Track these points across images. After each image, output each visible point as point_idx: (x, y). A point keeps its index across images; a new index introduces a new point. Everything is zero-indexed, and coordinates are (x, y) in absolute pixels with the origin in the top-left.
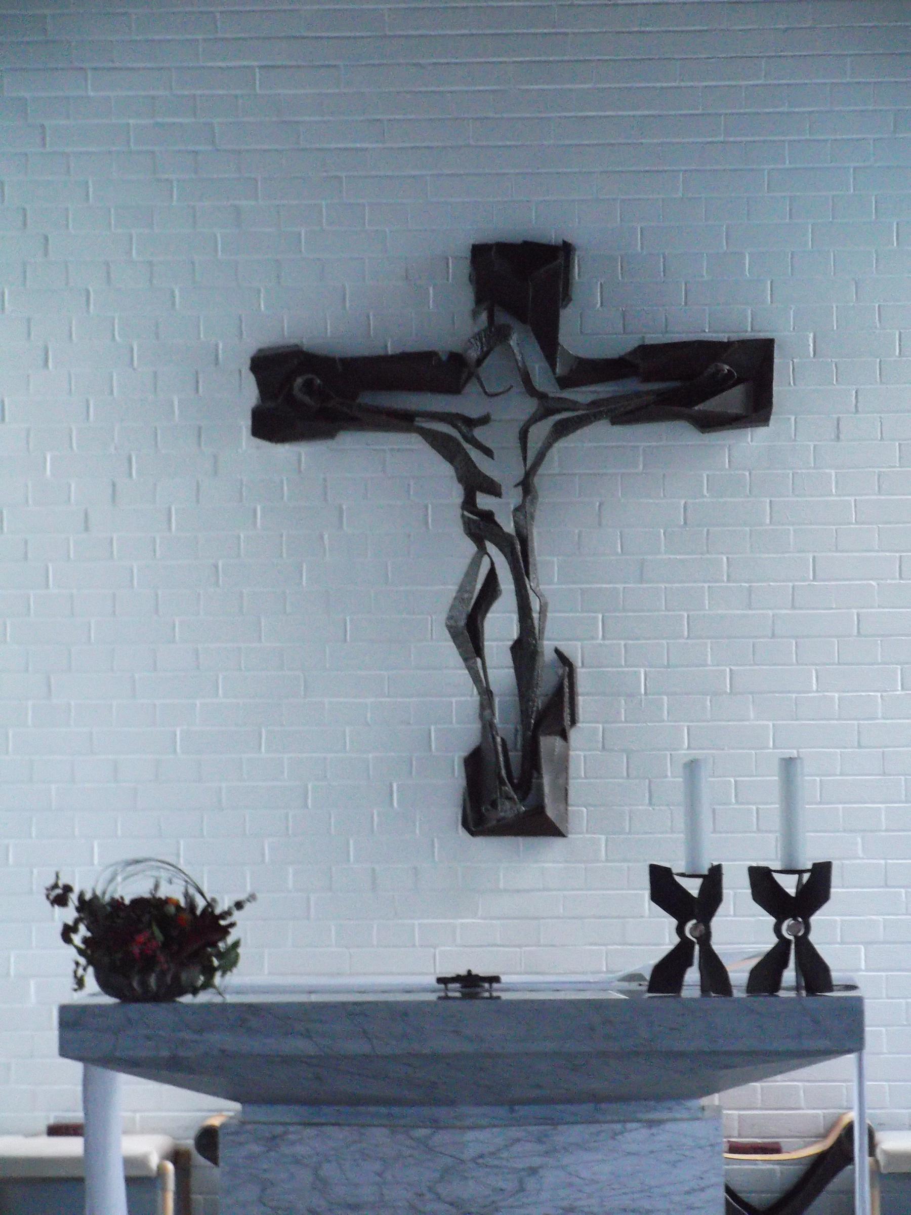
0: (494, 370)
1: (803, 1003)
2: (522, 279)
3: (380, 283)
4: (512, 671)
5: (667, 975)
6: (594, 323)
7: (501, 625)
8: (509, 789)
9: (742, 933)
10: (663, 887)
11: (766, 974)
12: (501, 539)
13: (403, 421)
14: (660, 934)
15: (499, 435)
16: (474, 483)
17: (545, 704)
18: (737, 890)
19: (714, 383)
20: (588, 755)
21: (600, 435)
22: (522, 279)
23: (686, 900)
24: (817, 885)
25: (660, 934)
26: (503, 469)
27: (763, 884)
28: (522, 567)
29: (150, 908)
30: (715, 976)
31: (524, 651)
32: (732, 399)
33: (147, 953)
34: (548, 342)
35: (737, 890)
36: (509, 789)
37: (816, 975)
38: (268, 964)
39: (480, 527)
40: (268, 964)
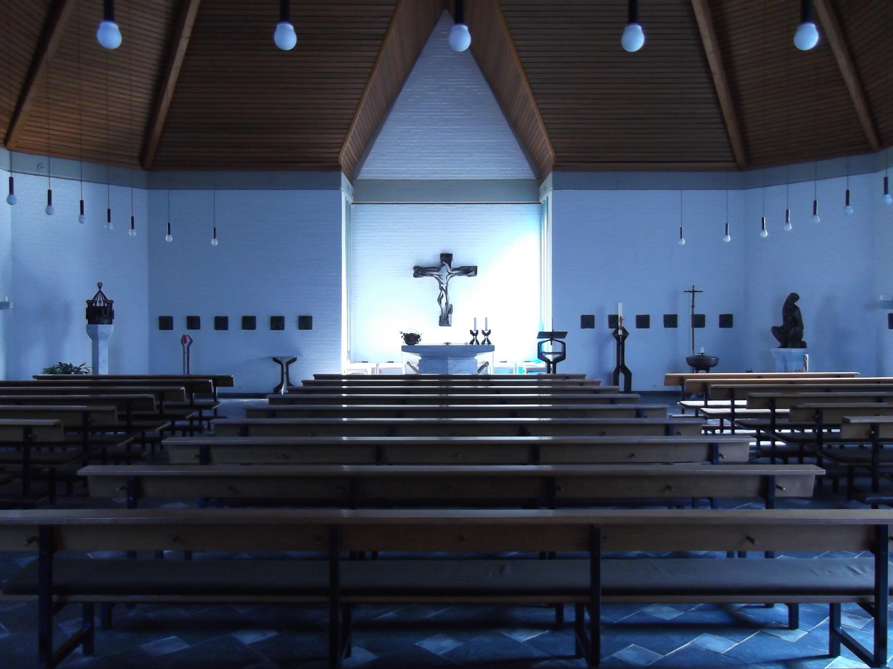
0: (443, 268)
1: (488, 347)
2: (447, 258)
3: (430, 257)
4: (730, 192)
5: (472, 342)
6: (455, 263)
7: (444, 301)
8: (444, 320)
9: (481, 338)
10: (472, 332)
11: (483, 342)
12: (444, 290)
13: (432, 275)
14: (471, 337)
15: (444, 277)
16: (441, 283)
17: (449, 310)
18: (480, 333)
19: (469, 271)
20: (454, 317)
21: (456, 277)
22: (447, 258)
23: (474, 334)
24: (489, 332)
25: (471, 337)
26: (444, 281)
27: (483, 332)
28: (446, 293)
29: (412, 335)
30: (477, 342)
31: (447, 303)
32: (473, 273)
33: (411, 340)
34: (450, 266)
35: (480, 333)
36: (444, 320)
37: (489, 343)
38: (423, 342)
39: (441, 288)
40: (423, 342)
